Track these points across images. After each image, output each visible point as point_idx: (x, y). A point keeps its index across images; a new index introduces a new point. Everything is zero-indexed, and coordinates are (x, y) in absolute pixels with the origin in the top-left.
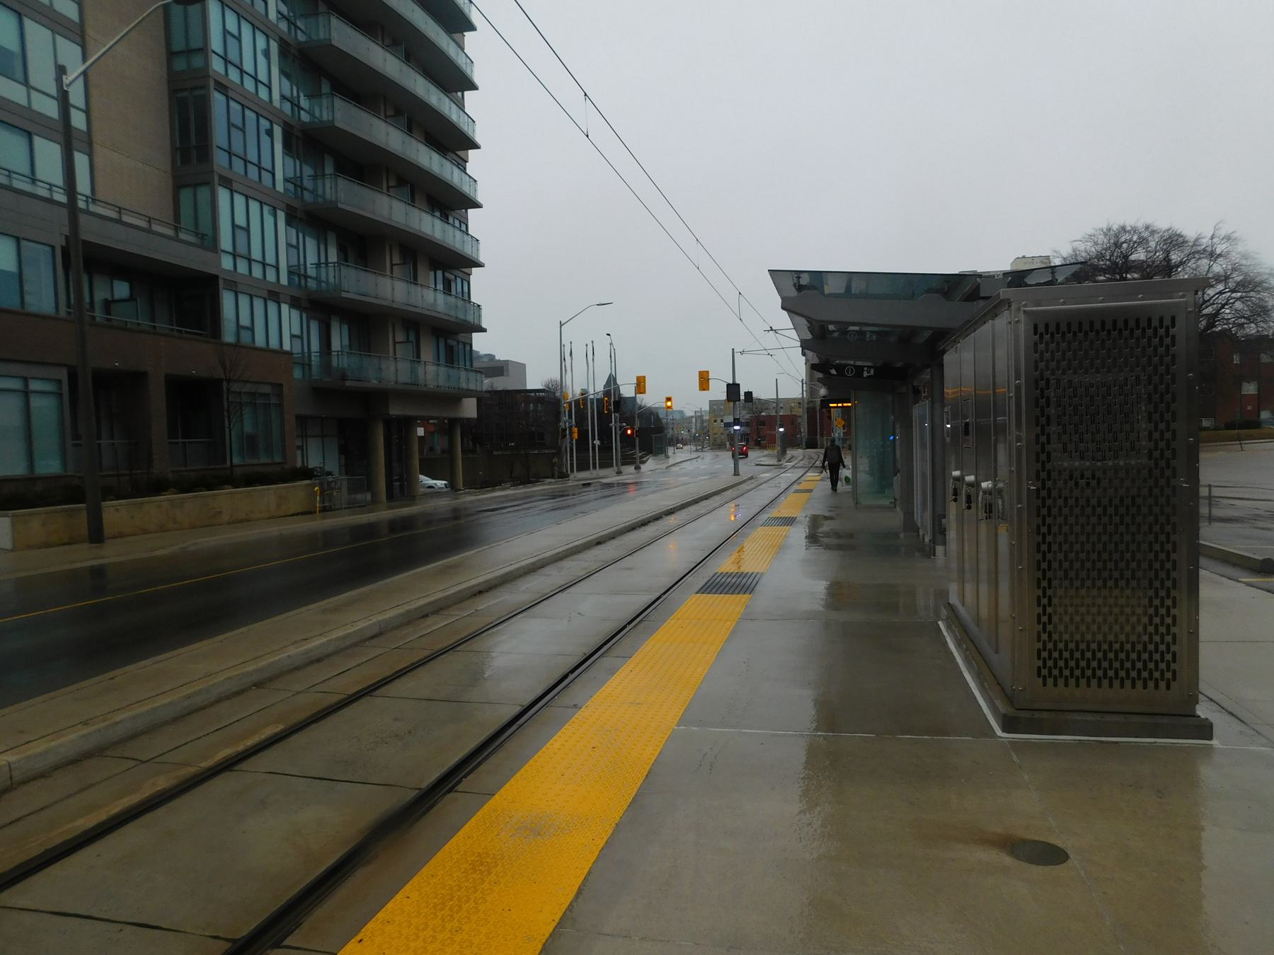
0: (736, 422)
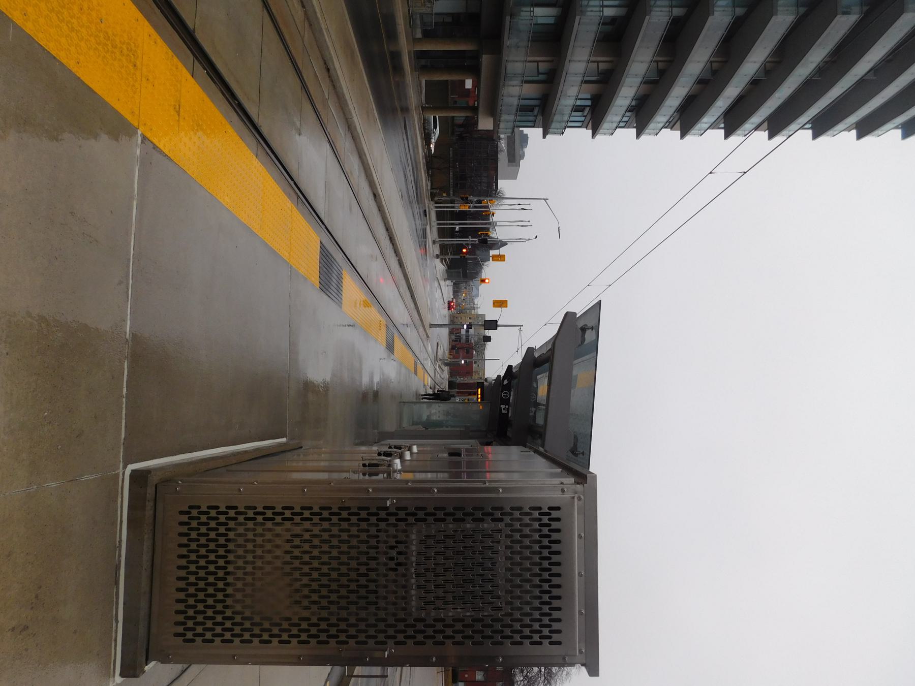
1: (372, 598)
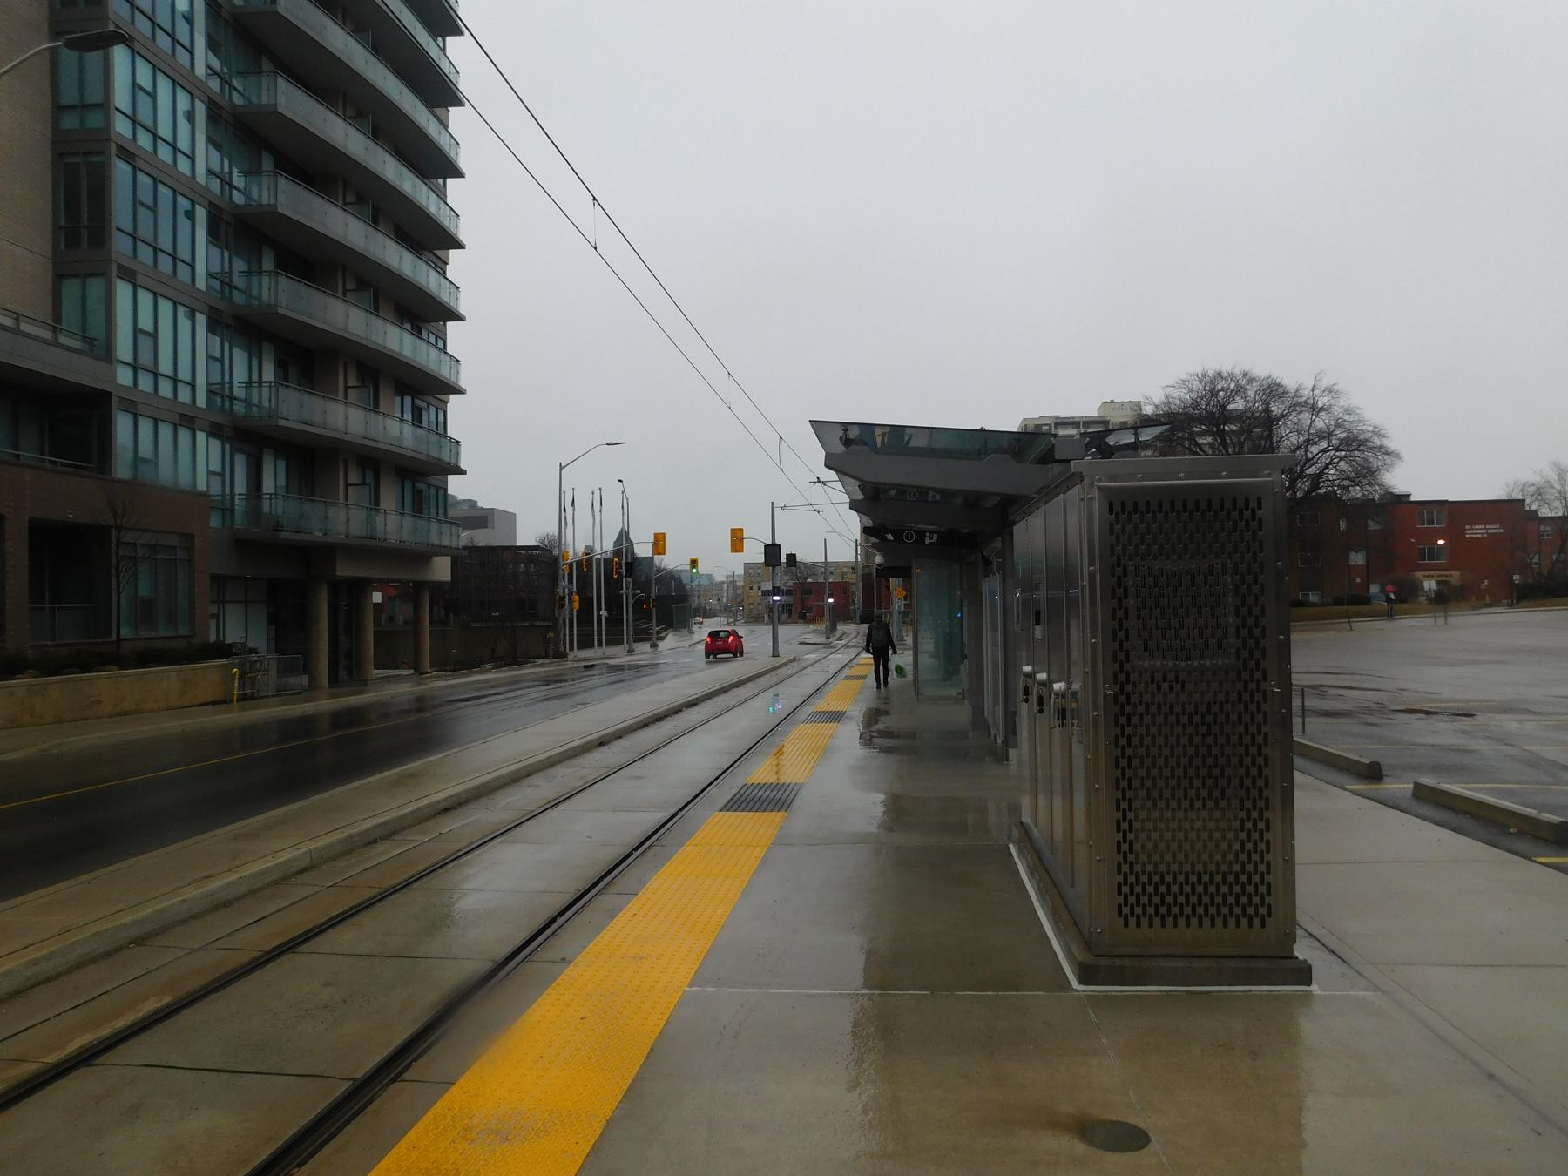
0: (776, 591)
1: (1215, 708)
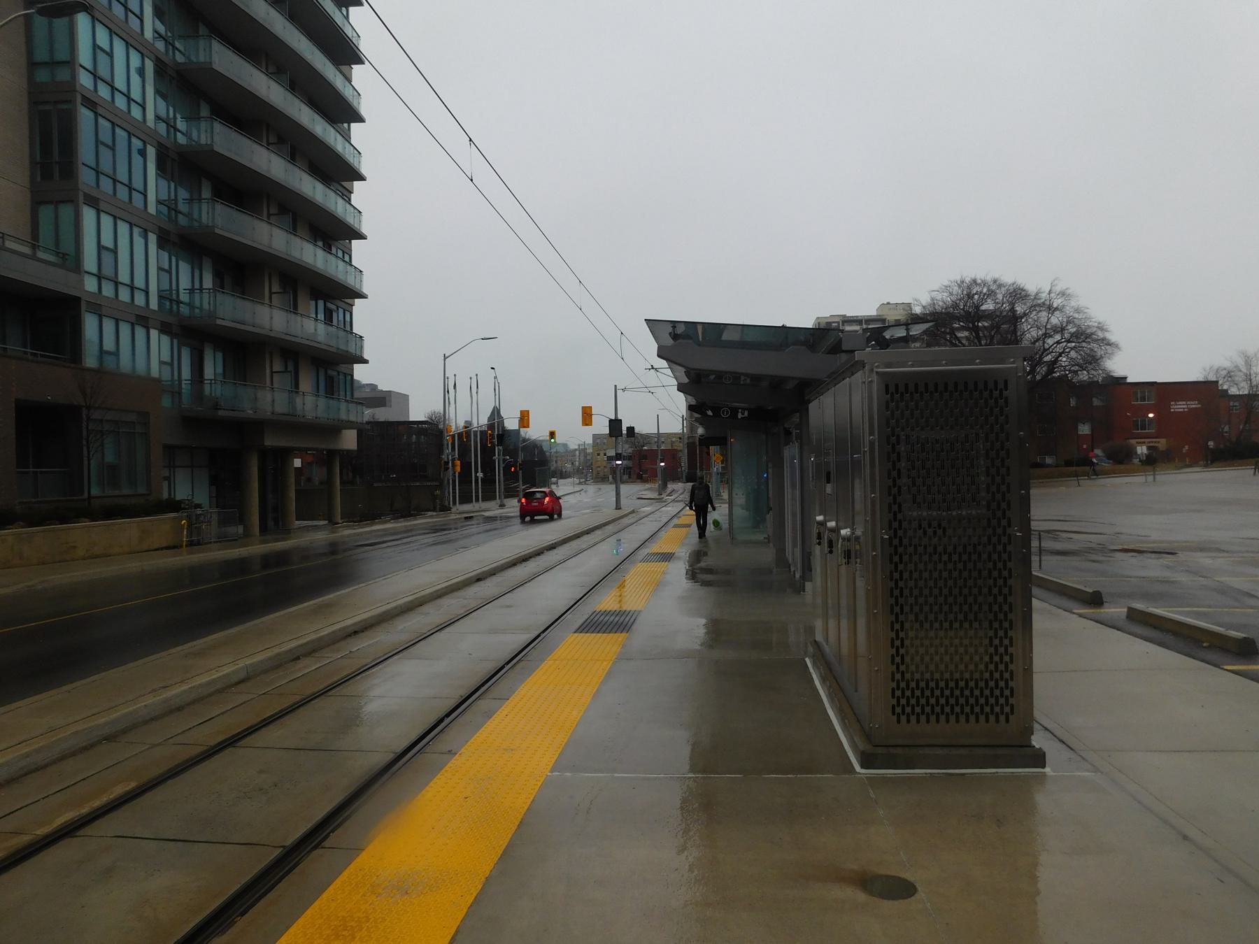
0: (618, 457)
